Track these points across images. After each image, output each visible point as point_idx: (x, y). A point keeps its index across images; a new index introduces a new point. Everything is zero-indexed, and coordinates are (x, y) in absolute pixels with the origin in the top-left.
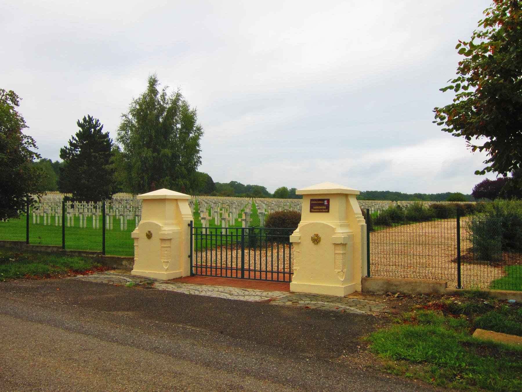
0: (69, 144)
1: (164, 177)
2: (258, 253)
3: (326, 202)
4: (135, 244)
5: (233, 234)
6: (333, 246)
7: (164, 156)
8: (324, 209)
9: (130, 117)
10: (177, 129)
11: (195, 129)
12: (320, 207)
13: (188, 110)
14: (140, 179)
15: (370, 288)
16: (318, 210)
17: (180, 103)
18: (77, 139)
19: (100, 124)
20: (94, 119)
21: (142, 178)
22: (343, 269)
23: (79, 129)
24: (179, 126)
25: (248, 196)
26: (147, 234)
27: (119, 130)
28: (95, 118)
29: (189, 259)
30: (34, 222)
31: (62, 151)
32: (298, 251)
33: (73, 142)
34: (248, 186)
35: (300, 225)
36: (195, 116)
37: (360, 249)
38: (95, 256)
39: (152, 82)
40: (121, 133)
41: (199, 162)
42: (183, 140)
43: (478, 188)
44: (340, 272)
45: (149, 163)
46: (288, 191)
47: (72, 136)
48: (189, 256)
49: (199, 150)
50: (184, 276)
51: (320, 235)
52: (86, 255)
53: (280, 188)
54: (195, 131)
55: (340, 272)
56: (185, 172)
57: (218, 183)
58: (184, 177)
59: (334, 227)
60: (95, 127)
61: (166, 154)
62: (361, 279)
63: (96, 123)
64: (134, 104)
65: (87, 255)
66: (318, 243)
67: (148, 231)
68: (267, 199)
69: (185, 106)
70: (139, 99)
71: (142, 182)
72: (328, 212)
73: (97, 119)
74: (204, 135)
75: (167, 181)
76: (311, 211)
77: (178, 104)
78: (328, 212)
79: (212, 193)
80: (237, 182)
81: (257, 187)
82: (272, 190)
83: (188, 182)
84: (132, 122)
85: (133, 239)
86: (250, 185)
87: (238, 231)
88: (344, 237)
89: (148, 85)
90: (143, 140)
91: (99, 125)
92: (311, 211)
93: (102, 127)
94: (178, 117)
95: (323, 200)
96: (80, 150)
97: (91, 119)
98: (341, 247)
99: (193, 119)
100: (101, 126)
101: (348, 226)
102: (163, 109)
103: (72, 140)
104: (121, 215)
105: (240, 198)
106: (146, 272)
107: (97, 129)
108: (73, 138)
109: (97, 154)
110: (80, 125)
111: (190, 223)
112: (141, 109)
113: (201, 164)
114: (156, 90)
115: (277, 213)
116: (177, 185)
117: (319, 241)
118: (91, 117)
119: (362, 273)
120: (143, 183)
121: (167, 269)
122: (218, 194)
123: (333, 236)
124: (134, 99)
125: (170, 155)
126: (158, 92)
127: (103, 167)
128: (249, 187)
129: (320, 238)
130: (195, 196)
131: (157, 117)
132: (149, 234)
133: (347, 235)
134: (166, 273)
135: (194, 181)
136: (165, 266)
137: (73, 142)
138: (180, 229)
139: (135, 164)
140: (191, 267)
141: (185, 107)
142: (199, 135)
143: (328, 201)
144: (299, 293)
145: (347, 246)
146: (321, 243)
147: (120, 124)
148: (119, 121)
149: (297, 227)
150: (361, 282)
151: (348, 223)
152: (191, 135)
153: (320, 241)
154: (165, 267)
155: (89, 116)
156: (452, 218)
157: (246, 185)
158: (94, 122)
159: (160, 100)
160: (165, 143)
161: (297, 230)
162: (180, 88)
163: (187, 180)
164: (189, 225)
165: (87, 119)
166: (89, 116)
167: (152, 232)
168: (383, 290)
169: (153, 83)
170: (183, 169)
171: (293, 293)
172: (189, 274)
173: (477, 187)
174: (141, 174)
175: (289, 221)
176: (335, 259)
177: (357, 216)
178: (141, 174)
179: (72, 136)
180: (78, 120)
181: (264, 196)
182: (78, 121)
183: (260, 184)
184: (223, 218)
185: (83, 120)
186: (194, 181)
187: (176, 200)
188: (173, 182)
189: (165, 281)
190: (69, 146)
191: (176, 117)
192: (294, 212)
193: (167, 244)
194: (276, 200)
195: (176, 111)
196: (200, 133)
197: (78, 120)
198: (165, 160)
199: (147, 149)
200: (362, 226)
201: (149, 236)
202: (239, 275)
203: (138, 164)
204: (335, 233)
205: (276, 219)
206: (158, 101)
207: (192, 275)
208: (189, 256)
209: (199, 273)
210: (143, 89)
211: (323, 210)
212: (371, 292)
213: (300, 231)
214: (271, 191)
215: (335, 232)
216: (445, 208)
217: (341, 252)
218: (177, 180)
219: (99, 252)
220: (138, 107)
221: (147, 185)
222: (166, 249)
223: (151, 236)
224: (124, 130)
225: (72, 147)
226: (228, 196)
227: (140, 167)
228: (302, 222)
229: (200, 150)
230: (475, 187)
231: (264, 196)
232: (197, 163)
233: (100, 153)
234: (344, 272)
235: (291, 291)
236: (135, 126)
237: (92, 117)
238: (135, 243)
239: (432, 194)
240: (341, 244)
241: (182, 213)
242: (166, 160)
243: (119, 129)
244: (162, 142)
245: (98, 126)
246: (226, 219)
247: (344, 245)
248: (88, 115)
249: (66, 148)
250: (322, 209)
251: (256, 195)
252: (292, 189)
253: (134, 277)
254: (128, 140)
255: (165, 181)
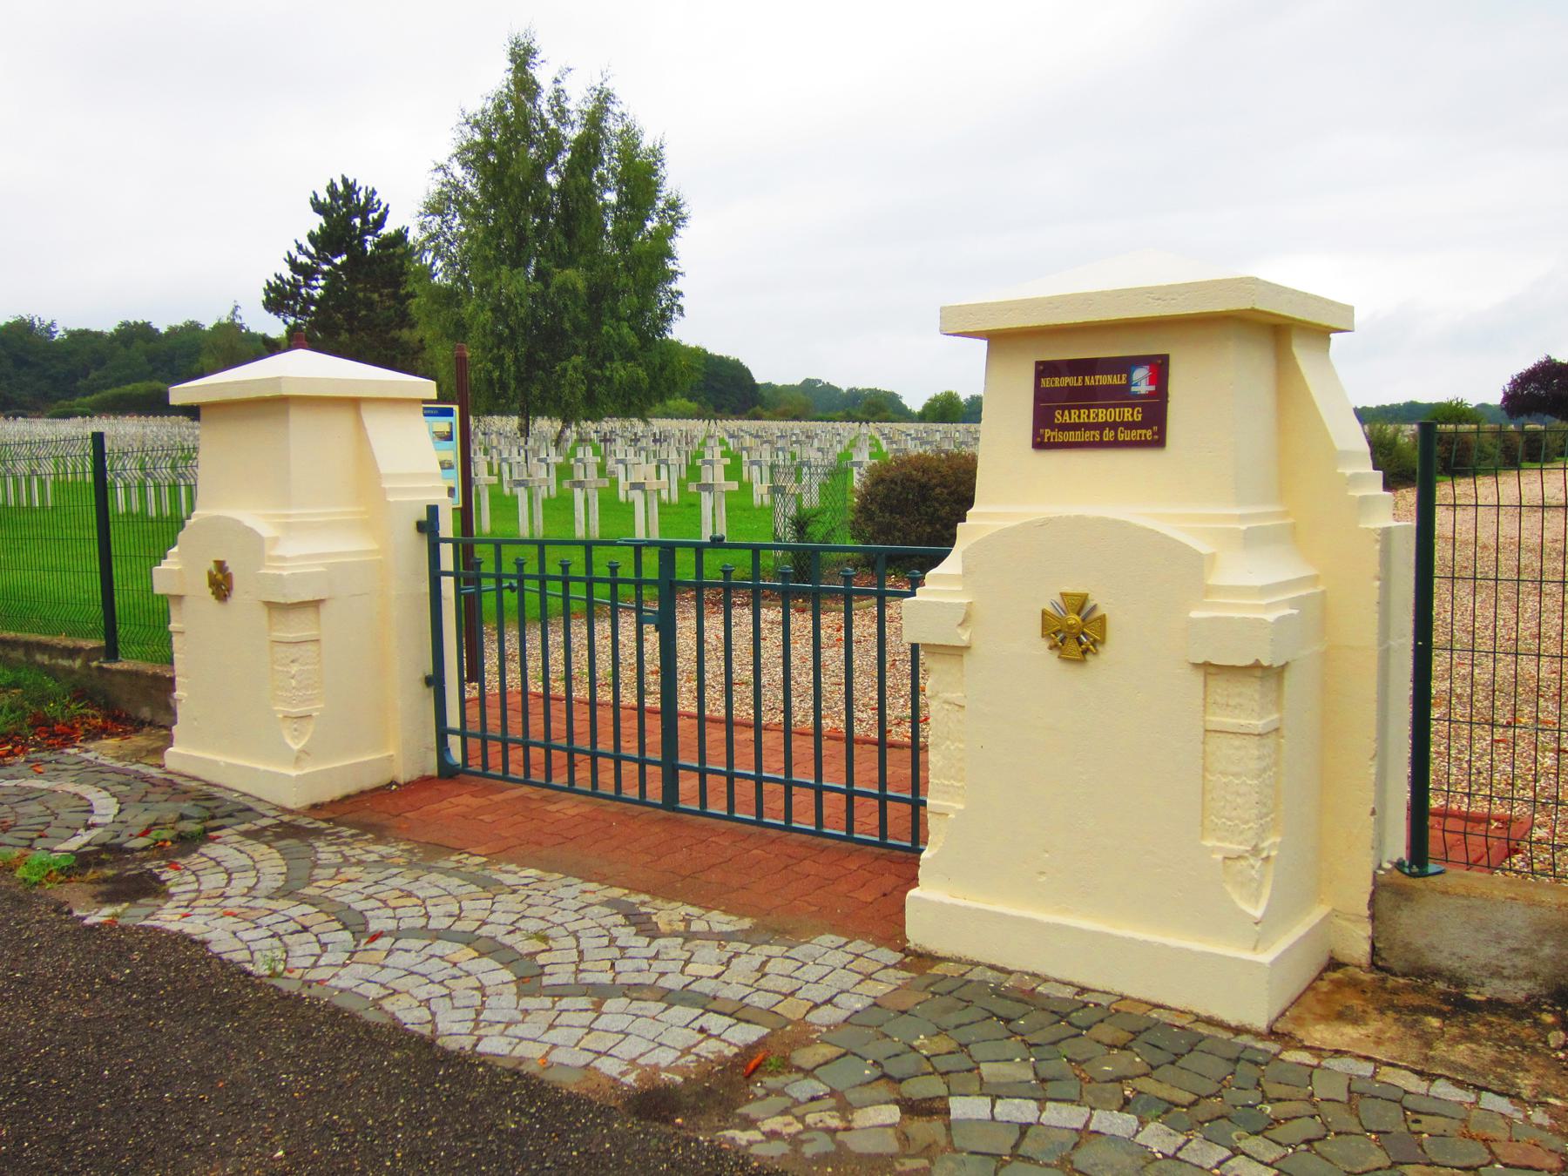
0: (288, 267)
1: (568, 357)
2: (831, 620)
3: (1141, 375)
4: (173, 626)
5: (621, 574)
6: (1197, 678)
7: (563, 289)
8: (1130, 426)
9: (459, 172)
10: (606, 206)
11: (660, 205)
12: (1103, 415)
13: (637, 146)
14: (490, 365)
15: (1432, 947)
16: (1088, 436)
17: (612, 125)
18: (312, 250)
19: (379, 203)
20: (360, 189)
21: (499, 361)
22: (1262, 833)
23: (316, 222)
24: (611, 197)
25: (850, 418)
26: (210, 573)
27: (421, 214)
28: (363, 182)
29: (430, 692)
30: (122, 508)
31: (270, 288)
32: (955, 696)
33: (299, 261)
34: (850, 391)
35: (970, 531)
36: (659, 164)
37: (1370, 688)
38: (78, 663)
39: (520, 56)
40: (430, 222)
41: (675, 308)
42: (623, 239)
43: (1519, 384)
44: (1239, 857)
45: (517, 316)
46: (959, 403)
47: (296, 241)
48: (429, 681)
49: (675, 273)
50: (403, 777)
51: (1103, 602)
52: (51, 658)
53: (939, 394)
54: (663, 211)
55: (1239, 857)
56: (633, 340)
57: (769, 386)
58: (629, 356)
59: (1204, 548)
60: (364, 211)
61: (570, 287)
62: (1368, 887)
63: (369, 200)
64: (467, 129)
65: (53, 661)
66: (1085, 652)
67: (216, 562)
68: (902, 426)
69: (628, 131)
70: (484, 112)
71: (496, 374)
72: (1159, 442)
73: (370, 189)
74: (689, 222)
75: (575, 368)
76: (1040, 444)
77: (603, 124)
78: (1159, 442)
79: (750, 412)
80: (820, 381)
81: (875, 392)
82: (915, 402)
83: (641, 373)
84: (464, 188)
85: (165, 598)
86: (856, 390)
87: (644, 559)
88: (1279, 620)
89: (509, 65)
90: (495, 242)
91: (376, 206)
92: (1040, 444)
93: (386, 210)
94: (610, 162)
95: (1124, 365)
96: (322, 283)
97: (350, 188)
98: (1251, 691)
99: (655, 173)
100: (382, 210)
101: (1289, 536)
102: (554, 144)
103: (294, 253)
104: (520, 483)
105: (825, 423)
106: (215, 763)
107: (371, 220)
108: (300, 247)
109: (376, 296)
110: (318, 207)
111: (424, 517)
112: (489, 145)
113: (682, 315)
114: (534, 82)
115: (905, 462)
116: (610, 380)
117: (1094, 643)
118: (351, 181)
119: (1379, 844)
120: (501, 376)
121: (303, 751)
122: (767, 414)
123: (1194, 614)
124: (463, 112)
125: (581, 285)
126: (539, 87)
127: (395, 333)
128: (855, 396)
129: (1103, 619)
130: (707, 421)
131: (539, 170)
132: (220, 577)
133: (1292, 603)
134: (293, 773)
135: (662, 369)
136: (294, 737)
137: (299, 261)
138: (376, 547)
139: (473, 317)
140: (442, 733)
141: (630, 139)
142: (675, 223)
143: (1159, 368)
144: (958, 961)
145: (1290, 679)
146: (1108, 652)
147: (424, 194)
148: (427, 186)
149: (943, 540)
150: (1372, 903)
151: (1285, 514)
152: (650, 225)
153: (1103, 642)
154: (289, 741)
155: (345, 181)
156: (1464, 474)
157: (845, 389)
158: (362, 195)
159: (547, 116)
160: (565, 249)
161: (951, 565)
162: (609, 73)
163: (640, 365)
164: (421, 527)
165: (341, 188)
166: (345, 181)
167: (232, 567)
168: (1532, 975)
169: (522, 57)
170: (626, 330)
171: (922, 960)
172: (432, 768)
173: (1516, 380)
174: (495, 351)
175: (946, 491)
176: (1205, 769)
177: (1349, 472)
178: (495, 351)
179: (296, 241)
180: (314, 193)
181: (894, 416)
182: (313, 196)
183: (884, 386)
184: (705, 484)
185: (328, 191)
186: (662, 369)
187: (355, 403)
188: (597, 372)
189: (291, 812)
190: (288, 274)
191: (601, 170)
192: (964, 457)
193: (297, 628)
194: (922, 426)
195: (597, 149)
196: (678, 218)
197: (314, 193)
198: (566, 305)
199: (511, 271)
200: (1386, 533)
201: (221, 584)
202: (655, 791)
203: (482, 318)
204: (1210, 590)
205: (896, 484)
206: (541, 115)
207: (447, 772)
208: (429, 681)
209: (475, 765)
210: (497, 76)
211: (1123, 436)
212: (1437, 974)
213: (967, 572)
214: (915, 404)
215: (1210, 582)
216: (1466, 443)
217: (1258, 724)
218: (608, 364)
219: (91, 649)
220: (478, 138)
221: (513, 384)
222: (294, 651)
223: (229, 589)
224: (440, 213)
225: (296, 276)
226: (796, 418)
227: (488, 327)
228: (979, 515)
229: (680, 271)
230: (1509, 381)
231: (894, 416)
232: (668, 313)
233: (386, 291)
234: (1268, 858)
235: (911, 945)
236: (472, 201)
237: (355, 181)
238: (173, 618)
239: (1364, 408)
240: (1257, 666)
241: (380, 466)
242: (569, 303)
243: (422, 210)
244: (556, 247)
245: (375, 211)
246: (716, 488)
247: (1267, 674)
248: (343, 176)
249: (280, 278)
250: (1114, 426)
251: (873, 414)
252: (972, 397)
253: (173, 787)
254: (452, 244)
255: (570, 372)
